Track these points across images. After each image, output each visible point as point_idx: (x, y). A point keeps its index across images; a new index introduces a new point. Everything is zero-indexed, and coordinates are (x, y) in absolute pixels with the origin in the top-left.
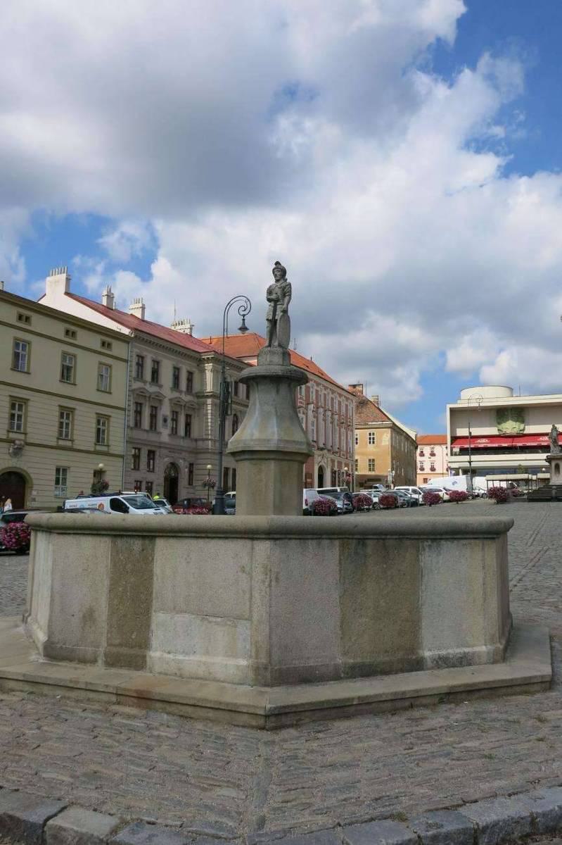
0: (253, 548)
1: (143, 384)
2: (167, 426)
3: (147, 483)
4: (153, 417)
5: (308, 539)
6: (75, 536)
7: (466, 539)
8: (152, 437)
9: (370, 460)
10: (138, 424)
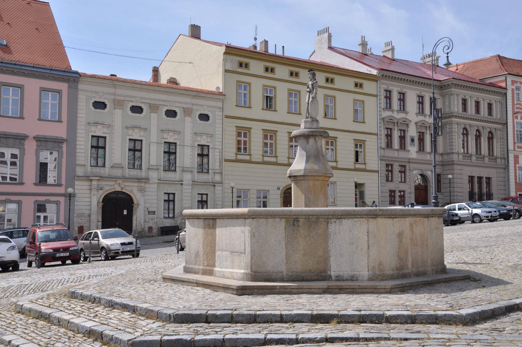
0: (245, 223)
1: (391, 112)
2: (414, 145)
3: (400, 192)
4: (402, 138)
5: (268, 218)
6: (193, 219)
7: (357, 218)
8: (402, 154)
10: (389, 145)
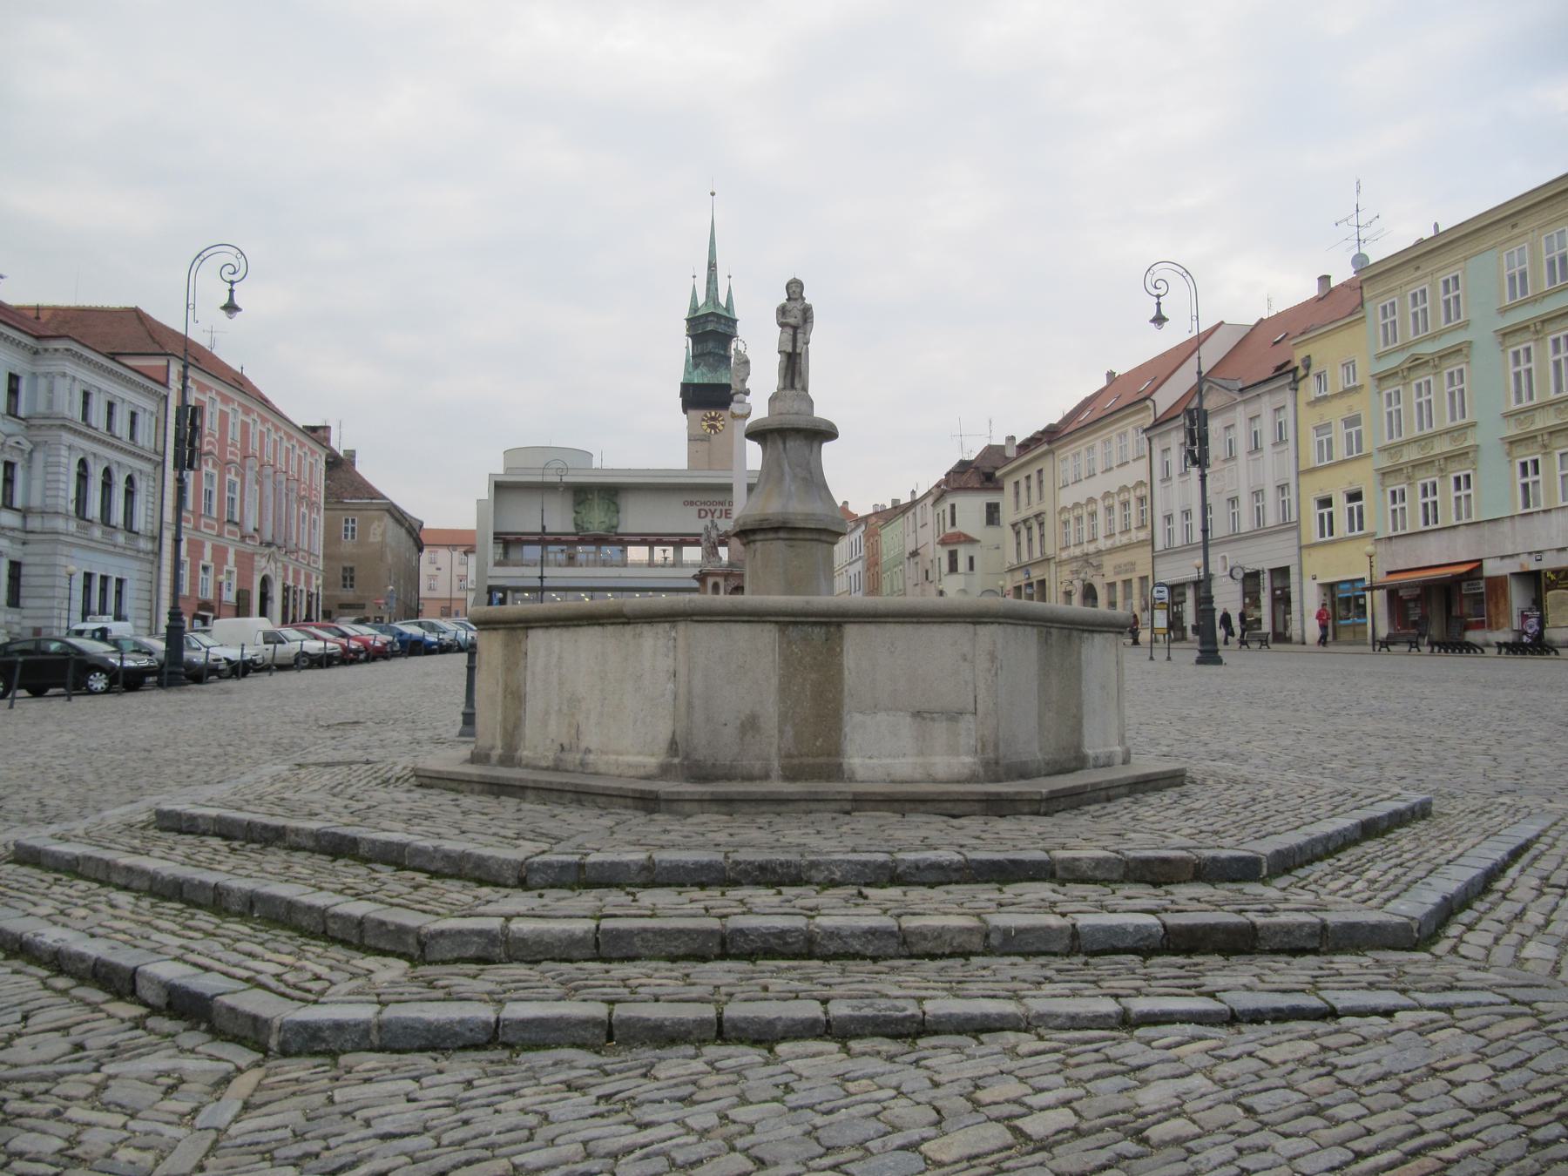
9: (345, 569)
